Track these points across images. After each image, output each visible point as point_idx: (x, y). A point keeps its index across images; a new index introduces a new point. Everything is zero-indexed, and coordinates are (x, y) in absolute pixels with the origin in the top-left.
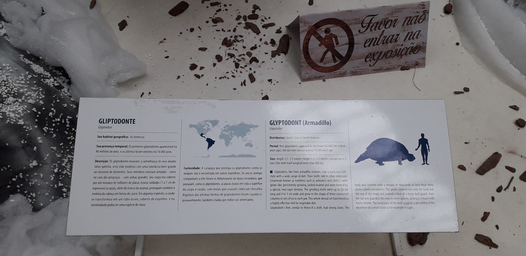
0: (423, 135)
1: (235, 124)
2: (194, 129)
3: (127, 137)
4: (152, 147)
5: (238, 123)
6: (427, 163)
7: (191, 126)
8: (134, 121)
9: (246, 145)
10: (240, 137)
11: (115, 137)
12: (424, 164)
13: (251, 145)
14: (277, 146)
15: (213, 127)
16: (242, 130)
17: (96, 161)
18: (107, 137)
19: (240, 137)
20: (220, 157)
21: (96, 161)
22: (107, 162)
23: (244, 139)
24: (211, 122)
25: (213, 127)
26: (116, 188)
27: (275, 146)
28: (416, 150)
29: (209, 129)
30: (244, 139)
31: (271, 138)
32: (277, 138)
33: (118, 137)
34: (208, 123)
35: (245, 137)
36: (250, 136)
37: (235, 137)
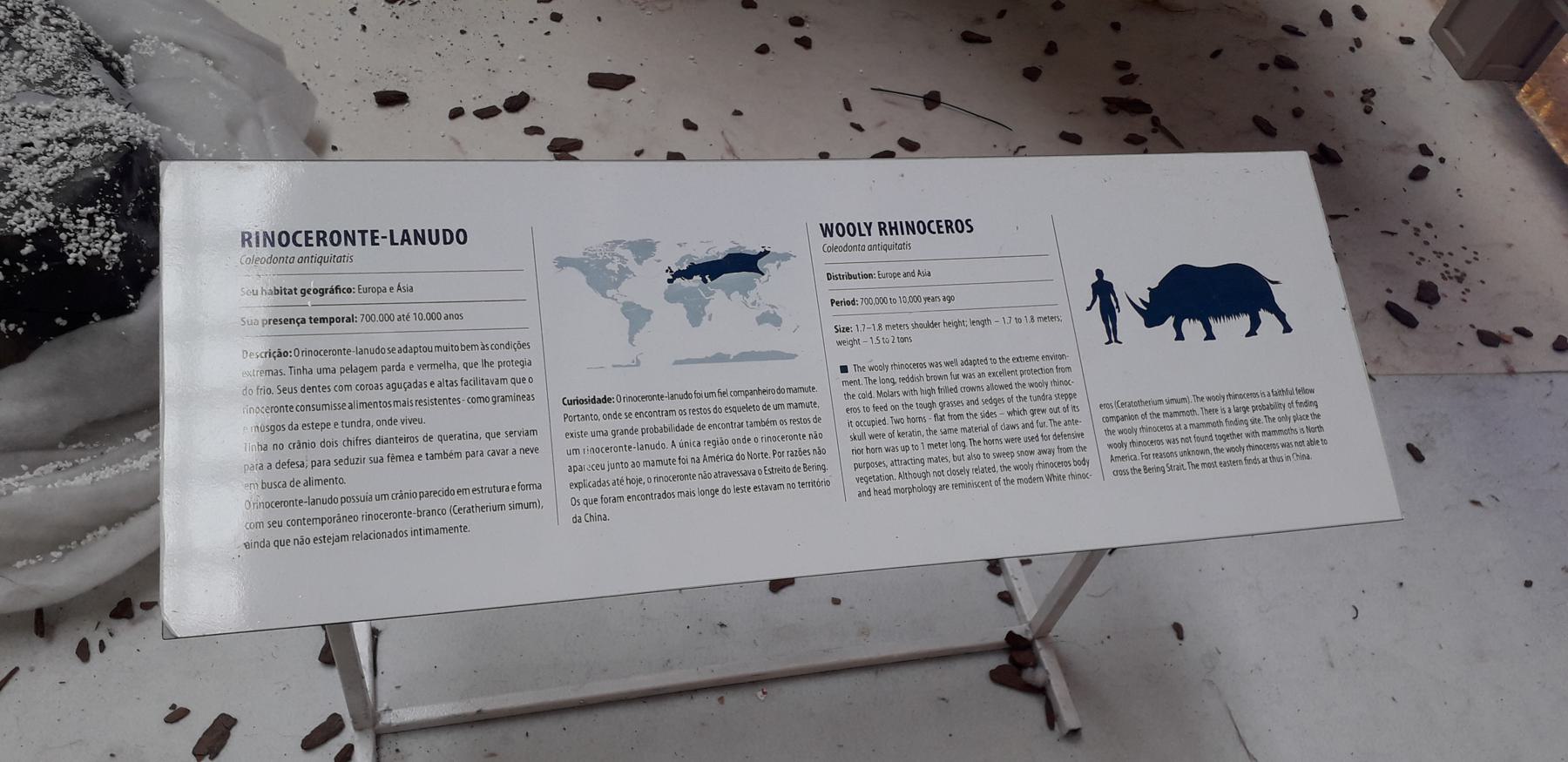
0: (1099, 273)
3: (349, 290)
4: (379, 350)
7: (562, 263)
8: (373, 238)
10: (736, 295)
11: (305, 292)
13: (776, 321)
14: (853, 302)
15: (639, 262)
19: (736, 295)
20: (677, 363)
23: (749, 301)
25: (639, 262)
27: (848, 303)
29: (624, 273)
31: (829, 277)
32: (850, 277)
34: (618, 250)
35: (752, 293)
36: (770, 285)
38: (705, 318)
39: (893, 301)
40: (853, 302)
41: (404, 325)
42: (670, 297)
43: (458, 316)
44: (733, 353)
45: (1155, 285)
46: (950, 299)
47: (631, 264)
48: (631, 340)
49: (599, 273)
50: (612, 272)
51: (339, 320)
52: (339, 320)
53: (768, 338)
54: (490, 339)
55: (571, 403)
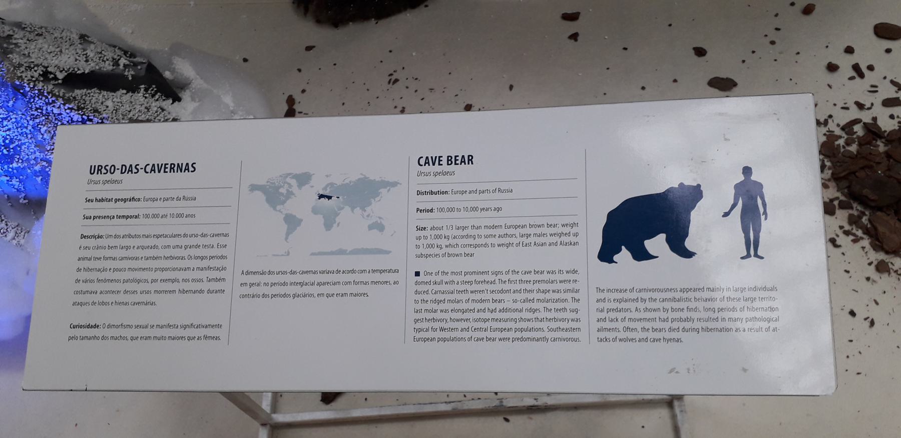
0: (747, 171)
1: (347, 181)
2: (258, 194)
5: (354, 177)
6: (756, 255)
7: (254, 188)
9: (371, 227)
10: (358, 210)
12: (748, 256)
13: (380, 227)
14: (432, 211)
16: (363, 192)
17: (83, 237)
18: (102, 200)
19: (358, 210)
20: (313, 254)
21: (83, 237)
22: (101, 237)
23: (366, 214)
24: (296, 177)
26: (150, 281)
27: (428, 211)
28: (726, 215)
29: (290, 194)
30: (366, 214)
32: (432, 193)
33: (122, 200)
34: (288, 180)
35: (368, 209)
36: (379, 208)
37: (347, 209)
38: (335, 225)
39: (459, 210)
40: (432, 211)
41: (164, 220)
42: (315, 211)
43: (193, 216)
44: (349, 249)
45: (687, 183)
46: (498, 209)
47: (295, 189)
48: (286, 239)
49: (274, 195)
50: (282, 194)
51: (131, 217)
52: (131, 217)
53: (374, 240)
54: (208, 230)
55: (248, 273)
